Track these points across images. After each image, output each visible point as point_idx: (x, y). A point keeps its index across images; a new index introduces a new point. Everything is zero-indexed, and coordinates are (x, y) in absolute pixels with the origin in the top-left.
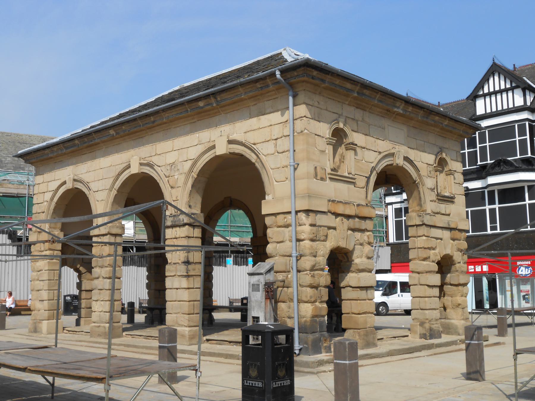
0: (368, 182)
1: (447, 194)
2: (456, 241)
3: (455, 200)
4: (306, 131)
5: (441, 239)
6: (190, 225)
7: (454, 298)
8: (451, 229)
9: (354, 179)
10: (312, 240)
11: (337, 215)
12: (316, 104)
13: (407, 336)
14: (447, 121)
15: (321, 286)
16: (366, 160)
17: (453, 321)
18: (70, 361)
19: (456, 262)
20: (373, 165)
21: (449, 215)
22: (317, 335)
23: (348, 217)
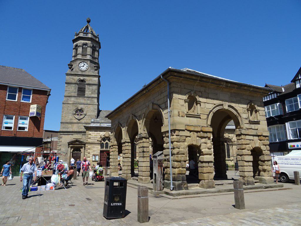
0: (208, 117)
1: (256, 120)
3: (260, 123)
7: (263, 167)
8: (258, 136)
9: (200, 116)
11: (191, 131)
15: (182, 161)
20: (211, 109)
22: (180, 182)
23: (197, 132)
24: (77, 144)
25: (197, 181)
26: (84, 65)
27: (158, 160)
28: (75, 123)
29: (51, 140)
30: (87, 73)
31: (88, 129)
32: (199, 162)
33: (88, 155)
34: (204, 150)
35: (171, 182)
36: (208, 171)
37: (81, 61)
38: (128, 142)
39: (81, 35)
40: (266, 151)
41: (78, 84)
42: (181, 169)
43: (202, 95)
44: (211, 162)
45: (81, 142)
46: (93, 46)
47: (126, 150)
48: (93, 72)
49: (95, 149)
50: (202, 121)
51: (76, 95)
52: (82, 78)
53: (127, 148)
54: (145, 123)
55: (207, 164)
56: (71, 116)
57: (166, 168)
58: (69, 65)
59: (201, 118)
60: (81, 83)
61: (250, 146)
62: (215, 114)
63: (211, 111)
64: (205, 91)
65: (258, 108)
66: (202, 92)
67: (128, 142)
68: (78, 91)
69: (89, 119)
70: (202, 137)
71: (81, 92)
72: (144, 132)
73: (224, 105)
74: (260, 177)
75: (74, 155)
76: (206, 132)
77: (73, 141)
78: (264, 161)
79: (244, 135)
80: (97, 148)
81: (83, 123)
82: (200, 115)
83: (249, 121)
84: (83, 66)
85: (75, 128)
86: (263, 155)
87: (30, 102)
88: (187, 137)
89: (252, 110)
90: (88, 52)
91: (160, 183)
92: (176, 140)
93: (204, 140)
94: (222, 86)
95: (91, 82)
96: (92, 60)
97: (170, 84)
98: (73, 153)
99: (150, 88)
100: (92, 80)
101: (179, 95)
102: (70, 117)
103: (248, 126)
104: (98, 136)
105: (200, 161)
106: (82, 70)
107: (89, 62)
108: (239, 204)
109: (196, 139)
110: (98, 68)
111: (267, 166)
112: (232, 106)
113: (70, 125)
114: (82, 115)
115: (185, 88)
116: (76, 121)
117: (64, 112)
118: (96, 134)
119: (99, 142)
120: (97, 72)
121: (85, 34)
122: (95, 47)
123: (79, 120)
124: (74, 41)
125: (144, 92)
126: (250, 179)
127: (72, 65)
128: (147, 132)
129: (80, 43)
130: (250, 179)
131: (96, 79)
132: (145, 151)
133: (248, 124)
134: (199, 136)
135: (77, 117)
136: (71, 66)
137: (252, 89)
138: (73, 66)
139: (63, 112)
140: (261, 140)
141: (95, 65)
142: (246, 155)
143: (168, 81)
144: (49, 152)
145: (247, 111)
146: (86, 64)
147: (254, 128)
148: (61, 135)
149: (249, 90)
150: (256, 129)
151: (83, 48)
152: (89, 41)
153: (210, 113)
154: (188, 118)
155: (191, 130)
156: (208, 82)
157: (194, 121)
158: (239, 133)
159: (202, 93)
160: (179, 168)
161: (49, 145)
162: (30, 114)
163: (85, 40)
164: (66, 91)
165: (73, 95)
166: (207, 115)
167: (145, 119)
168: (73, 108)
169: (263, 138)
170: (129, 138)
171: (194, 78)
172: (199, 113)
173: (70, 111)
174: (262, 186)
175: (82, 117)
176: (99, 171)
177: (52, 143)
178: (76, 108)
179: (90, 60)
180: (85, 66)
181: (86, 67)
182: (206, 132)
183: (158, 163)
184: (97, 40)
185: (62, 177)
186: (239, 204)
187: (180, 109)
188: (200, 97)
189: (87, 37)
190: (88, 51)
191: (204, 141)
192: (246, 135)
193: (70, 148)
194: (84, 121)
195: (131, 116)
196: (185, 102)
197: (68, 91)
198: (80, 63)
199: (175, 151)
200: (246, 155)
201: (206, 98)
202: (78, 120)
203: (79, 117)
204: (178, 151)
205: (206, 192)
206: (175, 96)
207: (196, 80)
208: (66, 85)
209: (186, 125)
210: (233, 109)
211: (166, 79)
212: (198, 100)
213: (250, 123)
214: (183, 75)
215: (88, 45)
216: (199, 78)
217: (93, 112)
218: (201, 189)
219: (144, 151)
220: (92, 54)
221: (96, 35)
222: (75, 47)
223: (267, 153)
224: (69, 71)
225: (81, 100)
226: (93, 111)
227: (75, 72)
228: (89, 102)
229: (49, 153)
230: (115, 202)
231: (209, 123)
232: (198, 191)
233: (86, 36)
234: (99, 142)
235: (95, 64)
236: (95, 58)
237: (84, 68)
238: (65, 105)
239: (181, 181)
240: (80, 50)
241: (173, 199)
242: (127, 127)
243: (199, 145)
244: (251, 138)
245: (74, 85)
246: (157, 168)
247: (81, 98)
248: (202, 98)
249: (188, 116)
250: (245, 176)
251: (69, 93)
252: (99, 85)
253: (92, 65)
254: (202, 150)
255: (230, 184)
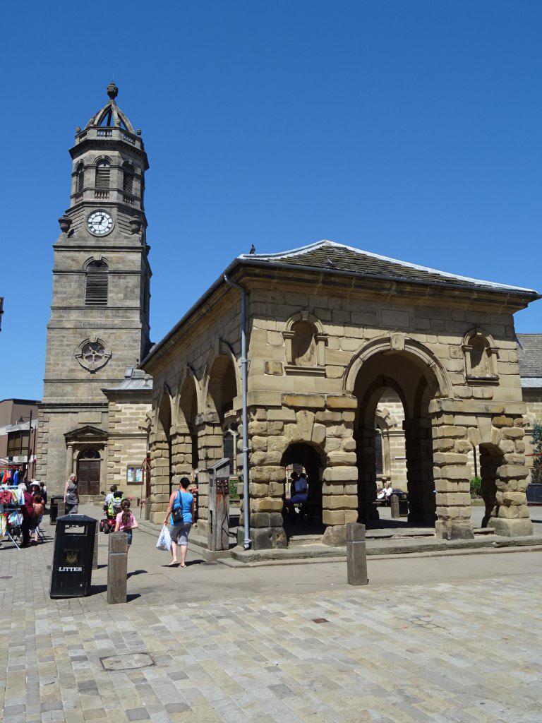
0: (347, 373)
2: (504, 429)
3: (500, 381)
7: (505, 493)
8: (493, 415)
9: (324, 370)
11: (297, 409)
13: (433, 535)
14: (476, 294)
15: (273, 481)
16: (344, 348)
20: (355, 353)
22: (266, 530)
23: (315, 410)
24: (88, 439)
25: (319, 528)
26: (103, 218)
27: (217, 479)
28: (82, 381)
29: (31, 427)
30: (110, 242)
31: (114, 396)
32: (323, 482)
33: (115, 467)
34: (333, 453)
35: (245, 530)
36: (340, 505)
37: (95, 209)
38: (184, 435)
39: (93, 135)
40: (515, 454)
41: (87, 273)
42: (269, 499)
43: (332, 317)
44: (350, 482)
45: (101, 432)
46: (126, 164)
47: (178, 453)
48: (126, 237)
49: (133, 451)
50: (329, 382)
51: (83, 305)
52: (97, 256)
53: (182, 448)
54: (209, 387)
55: (340, 488)
56: (70, 363)
58: (61, 221)
59: (328, 374)
60: (95, 269)
61: (467, 441)
62: (366, 364)
63: (357, 356)
64: (341, 308)
65: (494, 343)
66: (332, 311)
67: (184, 435)
69: (119, 368)
70: (328, 423)
71: (96, 295)
72: (209, 409)
73: (393, 341)
74: (498, 519)
75: (83, 468)
76: (341, 410)
77: (77, 430)
78: (506, 480)
79: (448, 413)
81: (104, 381)
82: (323, 368)
83: (467, 378)
84: (100, 223)
85: (83, 394)
86: (507, 463)
88: (286, 422)
89: (477, 350)
90: (112, 182)
91: (222, 533)
92: (259, 431)
93: (333, 430)
94: (387, 292)
95: (121, 267)
96: (124, 203)
97: (248, 294)
98: (78, 462)
99: (212, 301)
100: (123, 261)
101: (270, 322)
102: (68, 365)
103: (462, 391)
104: (141, 416)
105: (325, 481)
106: (97, 232)
107: (115, 211)
108: (358, 576)
110: (141, 224)
111: (515, 491)
112: (418, 343)
113: (68, 388)
114: (100, 357)
115: (285, 304)
116: (85, 375)
117: (53, 353)
118: (134, 411)
119: (145, 432)
120: (137, 236)
121: (103, 130)
122: (132, 167)
123: (93, 372)
124: (75, 152)
125: (204, 310)
126: (461, 524)
127: (70, 222)
128: (215, 411)
129: (89, 159)
130: (461, 524)
131: (136, 257)
132: (211, 456)
133: (464, 385)
134: (321, 419)
135: (86, 363)
136: (66, 224)
137: (475, 296)
138: (74, 224)
139: (49, 351)
140: (499, 427)
141: (133, 219)
142: (453, 464)
143: (244, 287)
144: (26, 461)
145: (461, 353)
146: (108, 216)
147: (481, 397)
148: (45, 415)
149: (469, 299)
151: (97, 172)
152: (114, 150)
153: (352, 361)
154: (291, 377)
155: (299, 405)
156: (350, 285)
157: (307, 384)
158: (438, 410)
159: (332, 313)
160: (263, 496)
161: (25, 439)
163: (104, 150)
164: (56, 293)
165: (74, 305)
166: (345, 367)
167: (208, 377)
168: (74, 341)
170: (186, 424)
171: (307, 276)
172: (322, 363)
173: (66, 348)
174: (491, 540)
175: (99, 363)
176: (114, 507)
177: (32, 435)
180: (105, 223)
182: (341, 410)
183: (217, 486)
184: (137, 145)
185: (10, 522)
186: (358, 576)
187: (271, 356)
188: (325, 322)
189: (108, 138)
190: (111, 179)
191: (334, 432)
192: (454, 414)
193: (70, 449)
194: (105, 374)
195: (186, 367)
196: (285, 338)
197: (61, 293)
198: (94, 212)
199: (255, 458)
200: (453, 464)
201: (344, 326)
202: (89, 373)
203: (91, 363)
204: (263, 458)
205: (328, 552)
206: (258, 324)
207: (317, 282)
208: (55, 277)
209: (285, 395)
211: (237, 283)
212: (320, 331)
213: (470, 384)
214: (276, 273)
215: (113, 163)
216: (321, 278)
217: (130, 350)
218: (324, 548)
219: (209, 456)
220: (124, 187)
221: (133, 132)
222: (78, 170)
223: (515, 460)
224: (61, 239)
225: (97, 317)
226: (130, 346)
227: (78, 240)
228: (117, 321)
230: (68, 565)
231: (350, 386)
232: (320, 550)
233: (106, 136)
234: (145, 432)
235: (132, 215)
236: (133, 199)
237: (101, 229)
238: (53, 333)
239: (270, 528)
240: (90, 177)
241: (237, 567)
242: (180, 396)
243: (319, 440)
244: (471, 420)
245: (76, 277)
246: (215, 499)
247: (95, 313)
248: (331, 326)
249: (293, 370)
250: (449, 517)
251: (63, 300)
252: (146, 274)
253: (123, 219)
254: (329, 455)
255: (412, 536)
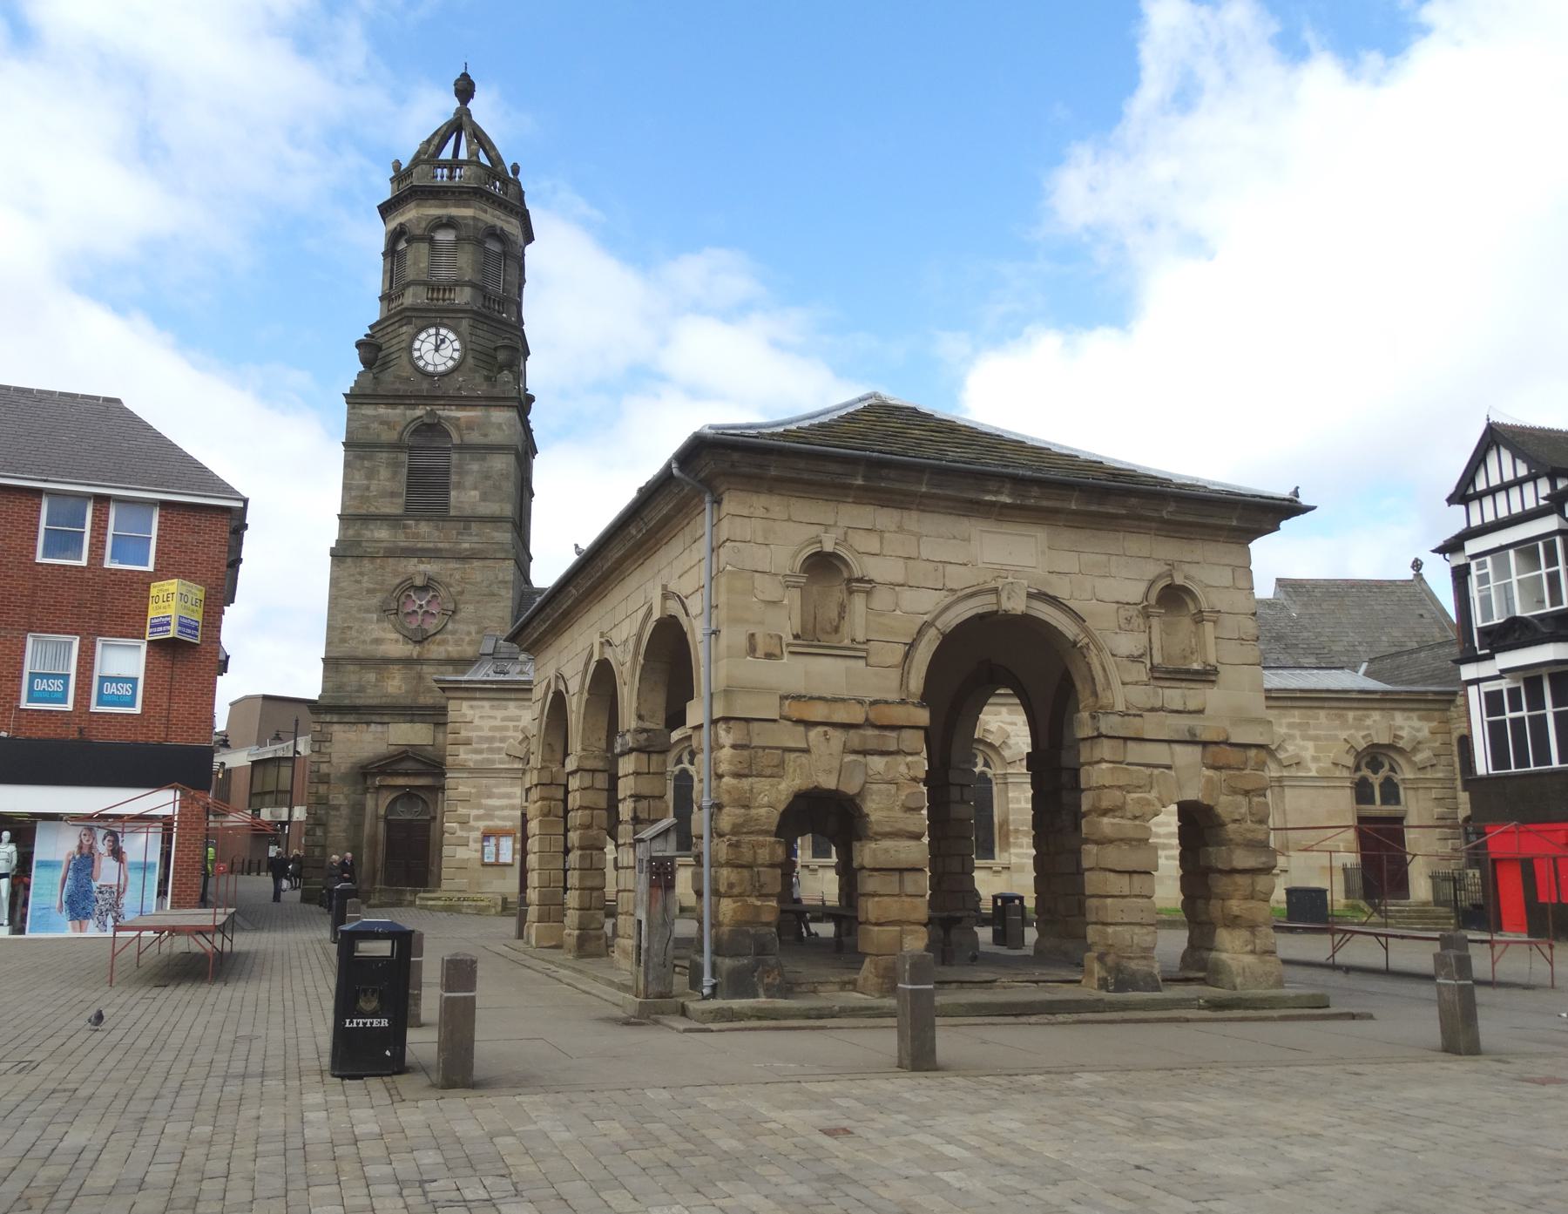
1: (1196, 666)
4: (729, 568)
5: (1169, 767)
6: (639, 750)
10: (737, 775)
11: (809, 724)
12: (760, 512)
17: (1224, 956)
18: (1513, 979)
19: (1227, 820)
21: (1201, 711)
29: (296, 752)
34: (876, 809)
57: (1226, 926)
63: (927, 625)
68: (409, 486)
80: (508, 796)
87: (150, 568)
95: (474, 437)
104: (510, 733)
109: (836, 764)
118: (498, 723)
146: (452, 336)
150: (1190, 712)
162: (148, 630)
169: (1234, 756)
178: (398, 581)
179: (472, 311)
181: (449, 352)
187: (761, 623)
194: (442, 649)
209: (786, 698)
210: (1051, 604)
229: (283, 824)
231: (916, 683)
244: (1159, 753)
